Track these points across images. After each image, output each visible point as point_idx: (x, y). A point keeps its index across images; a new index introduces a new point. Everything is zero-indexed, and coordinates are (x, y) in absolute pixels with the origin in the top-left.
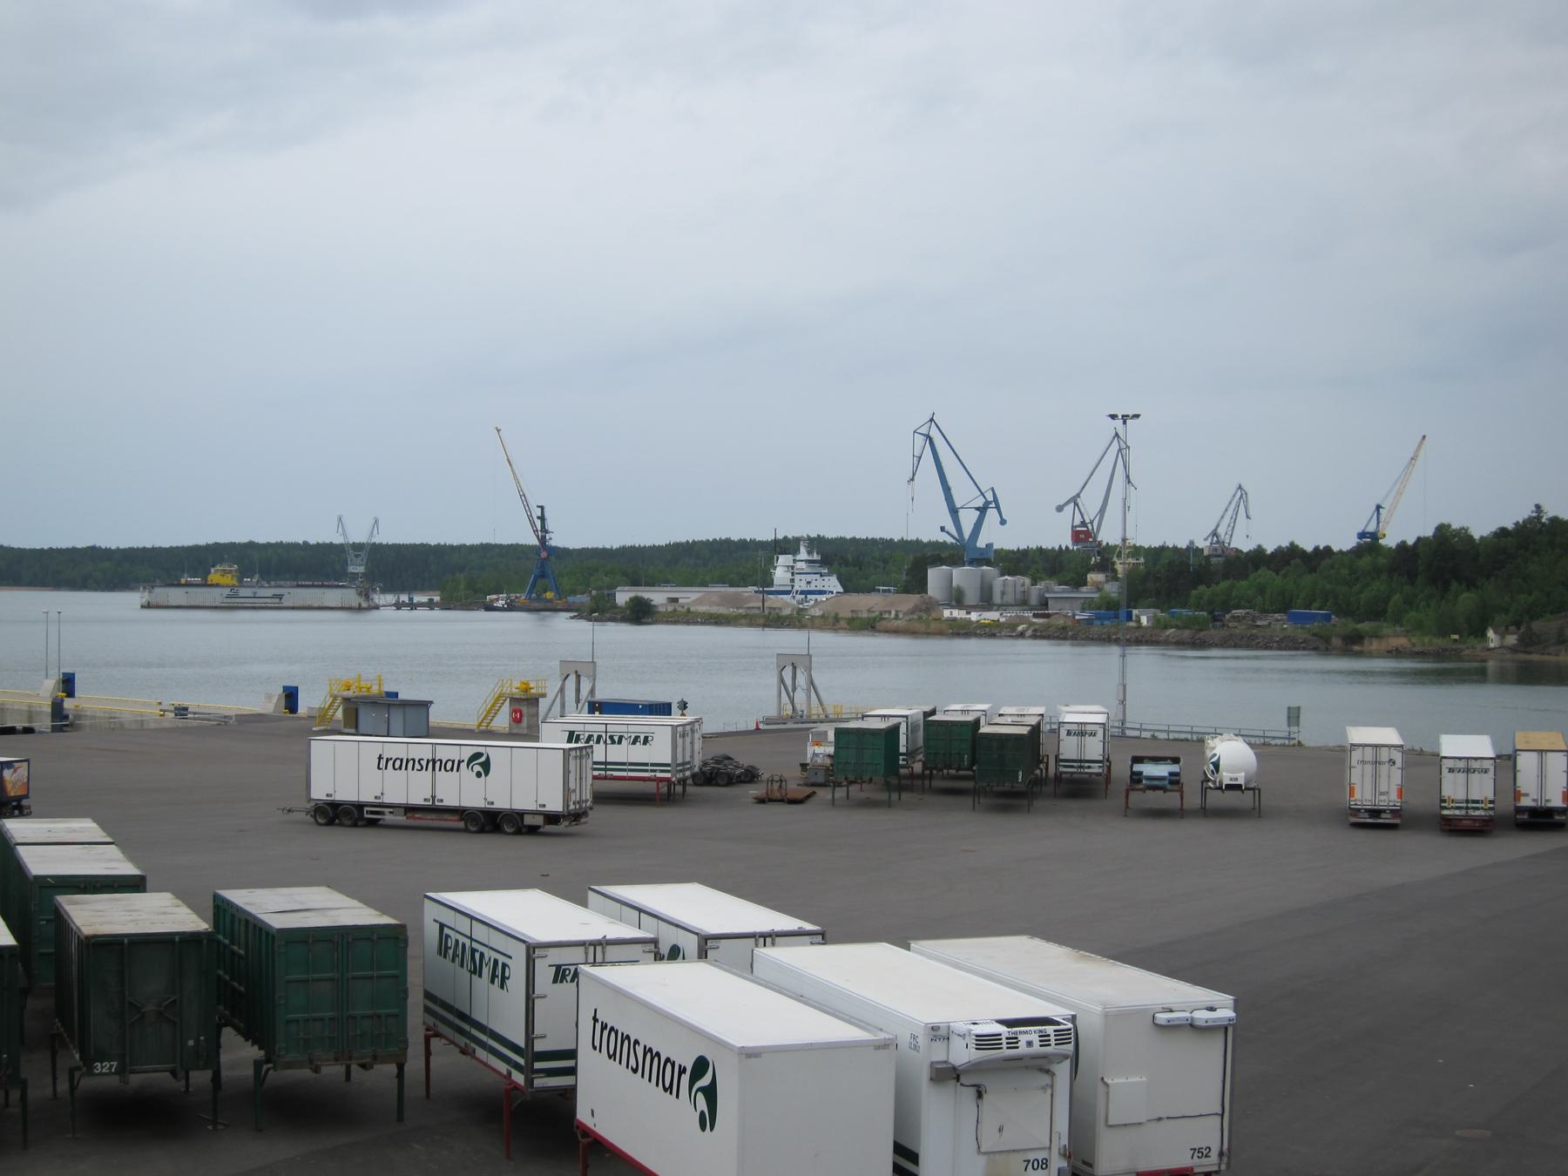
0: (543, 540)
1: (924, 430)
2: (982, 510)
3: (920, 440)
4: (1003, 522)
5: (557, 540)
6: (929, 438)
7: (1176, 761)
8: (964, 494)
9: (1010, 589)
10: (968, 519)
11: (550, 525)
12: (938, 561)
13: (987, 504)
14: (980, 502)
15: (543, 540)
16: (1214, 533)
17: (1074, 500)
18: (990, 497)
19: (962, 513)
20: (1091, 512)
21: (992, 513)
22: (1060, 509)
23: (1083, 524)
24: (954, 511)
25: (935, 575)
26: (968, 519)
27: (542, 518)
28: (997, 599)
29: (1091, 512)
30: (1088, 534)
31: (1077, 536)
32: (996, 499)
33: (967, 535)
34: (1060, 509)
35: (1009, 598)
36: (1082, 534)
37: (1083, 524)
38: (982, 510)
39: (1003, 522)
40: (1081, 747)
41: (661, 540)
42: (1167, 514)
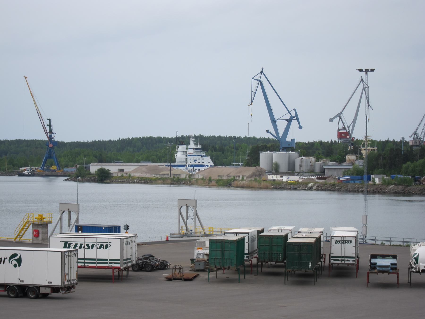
0: (50, 138)
1: (257, 78)
2: (289, 121)
3: (255, 83)
4: (300, 127)
5: (58, 137)
6: (260, 82)
8: (280, 112)
9: (304, 164)
10: (282, 126)
11: (54, 130)
12: (265, 148)
14: (288, 117)
15: (50, 138)
16: (415, 134)
17: (339, 116)
18: (293, 114)
19: (278, 123)
20: (348, 119)
21: (294, 123)
22: (331, 120)
23: (344, 128)
24: (274, 122)
26: (282, 126)
27: (50, 126)
28: (297, 169)
30: (346, 134)
31: (340, 135)
33: (281, 135)
34: (331, 120)
35: (304, 169)
36: (343, 134)
37: (344, 128)
38: (289, 121)
39: (300, 127)
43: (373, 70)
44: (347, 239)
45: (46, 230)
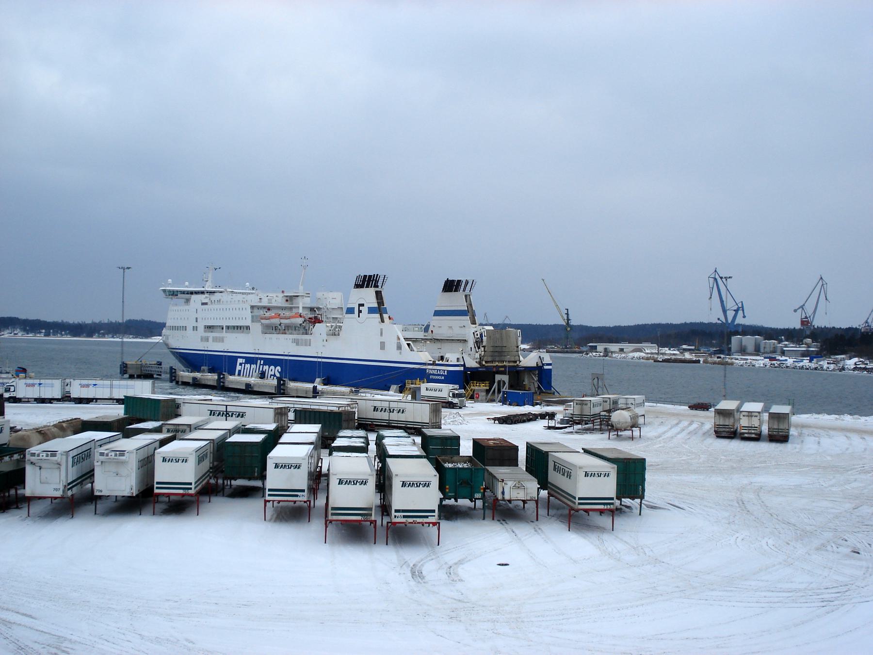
0: (568, 323)
1: (713, 276)
2: (737, 311)
3: (712, 280)
4: (744, 317)
5: (573, 322)
6: (715, 279)
7: (241, 415)
8: (730, 305)
9: (768, 346)
10: (730, 315)
11: (570, 317)
12: (736, 333)
13: (738, 308)
14: (736, 308)
15: (568, 323)
16: (867, 322)
17: (802, 307)
18: (740, 305)
19: (728, 312)
20: (809, 310)
21: (740, 312)
22: (795, 311)
23: (806, 317)
24: (725, 311)
25: (735, 339)
26: (730, 315)
27: (567, 314)
28: (762, 350)
29: (809, 310)
30: (808, 322)
31: (803, 323)
32: (742, 307)
33: (729, 321)
34: (795, 311)
35: (768, 350)
36: (805, 322)
37: (806, 317)
38: (737, 311)
39: (744, 317)
40: (582, 410)
41: (632, 323)
42: (838, 315)
43: (128, 268)
44: (181, 427)
45: (162, 404)
